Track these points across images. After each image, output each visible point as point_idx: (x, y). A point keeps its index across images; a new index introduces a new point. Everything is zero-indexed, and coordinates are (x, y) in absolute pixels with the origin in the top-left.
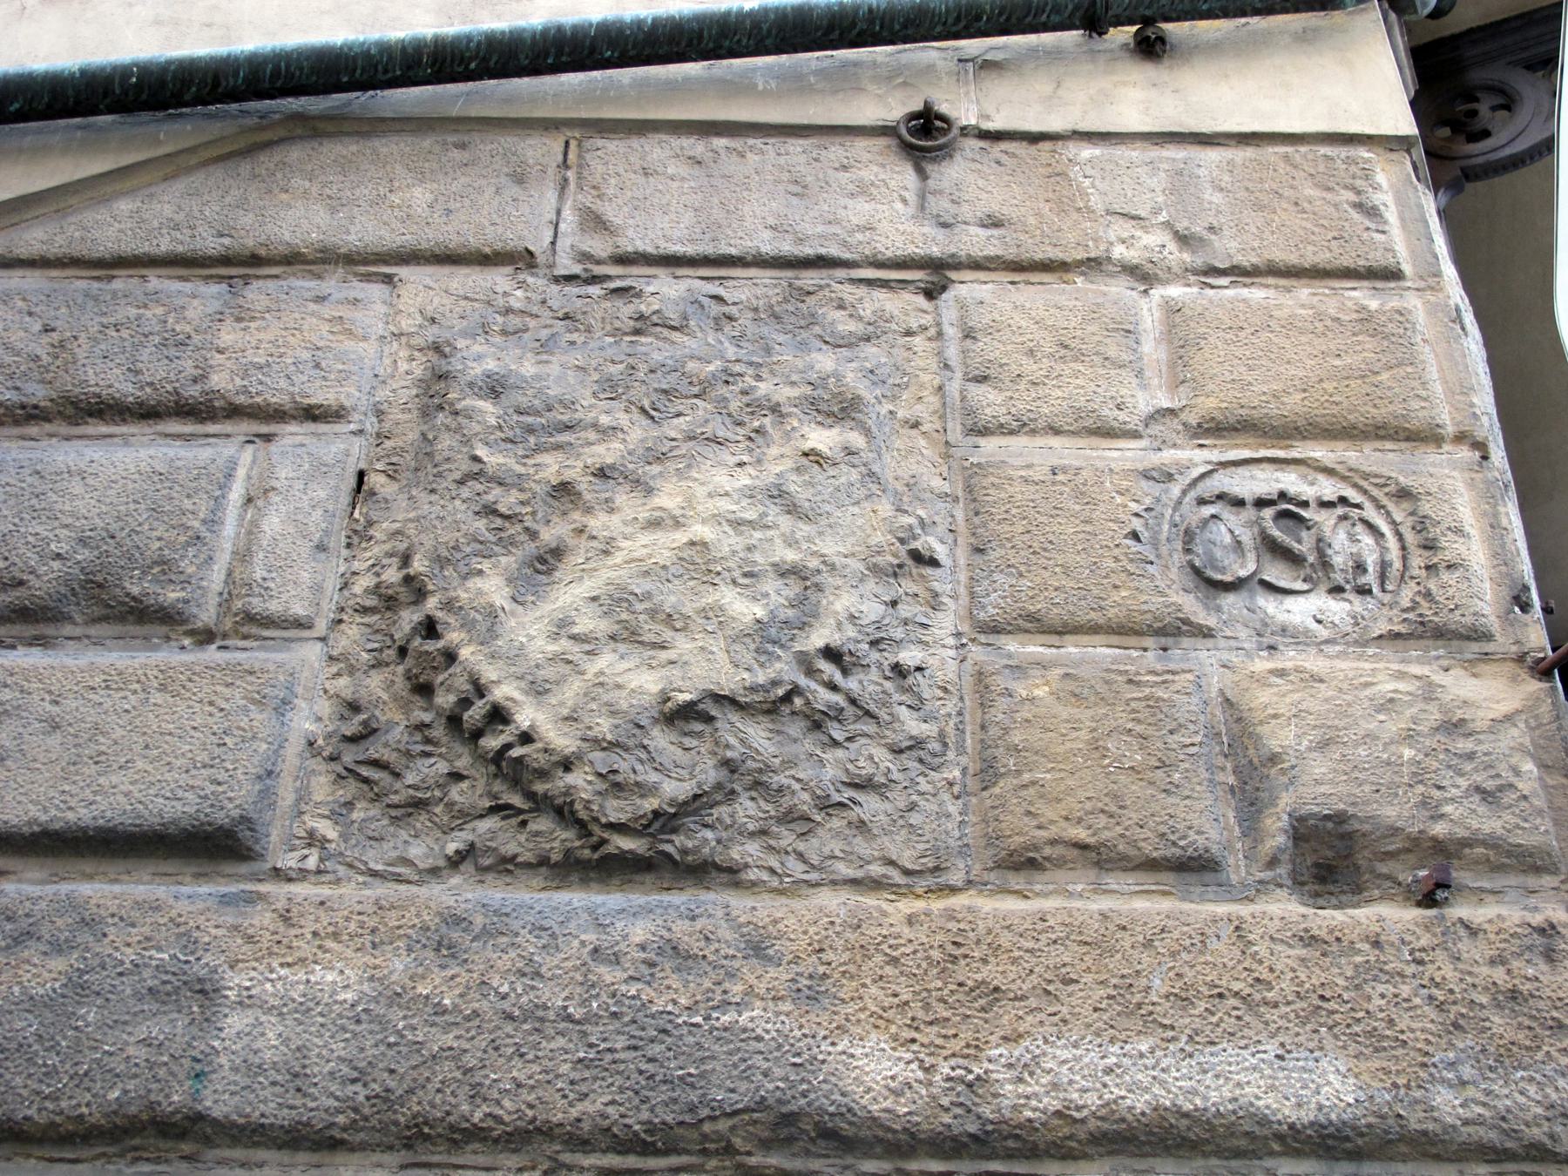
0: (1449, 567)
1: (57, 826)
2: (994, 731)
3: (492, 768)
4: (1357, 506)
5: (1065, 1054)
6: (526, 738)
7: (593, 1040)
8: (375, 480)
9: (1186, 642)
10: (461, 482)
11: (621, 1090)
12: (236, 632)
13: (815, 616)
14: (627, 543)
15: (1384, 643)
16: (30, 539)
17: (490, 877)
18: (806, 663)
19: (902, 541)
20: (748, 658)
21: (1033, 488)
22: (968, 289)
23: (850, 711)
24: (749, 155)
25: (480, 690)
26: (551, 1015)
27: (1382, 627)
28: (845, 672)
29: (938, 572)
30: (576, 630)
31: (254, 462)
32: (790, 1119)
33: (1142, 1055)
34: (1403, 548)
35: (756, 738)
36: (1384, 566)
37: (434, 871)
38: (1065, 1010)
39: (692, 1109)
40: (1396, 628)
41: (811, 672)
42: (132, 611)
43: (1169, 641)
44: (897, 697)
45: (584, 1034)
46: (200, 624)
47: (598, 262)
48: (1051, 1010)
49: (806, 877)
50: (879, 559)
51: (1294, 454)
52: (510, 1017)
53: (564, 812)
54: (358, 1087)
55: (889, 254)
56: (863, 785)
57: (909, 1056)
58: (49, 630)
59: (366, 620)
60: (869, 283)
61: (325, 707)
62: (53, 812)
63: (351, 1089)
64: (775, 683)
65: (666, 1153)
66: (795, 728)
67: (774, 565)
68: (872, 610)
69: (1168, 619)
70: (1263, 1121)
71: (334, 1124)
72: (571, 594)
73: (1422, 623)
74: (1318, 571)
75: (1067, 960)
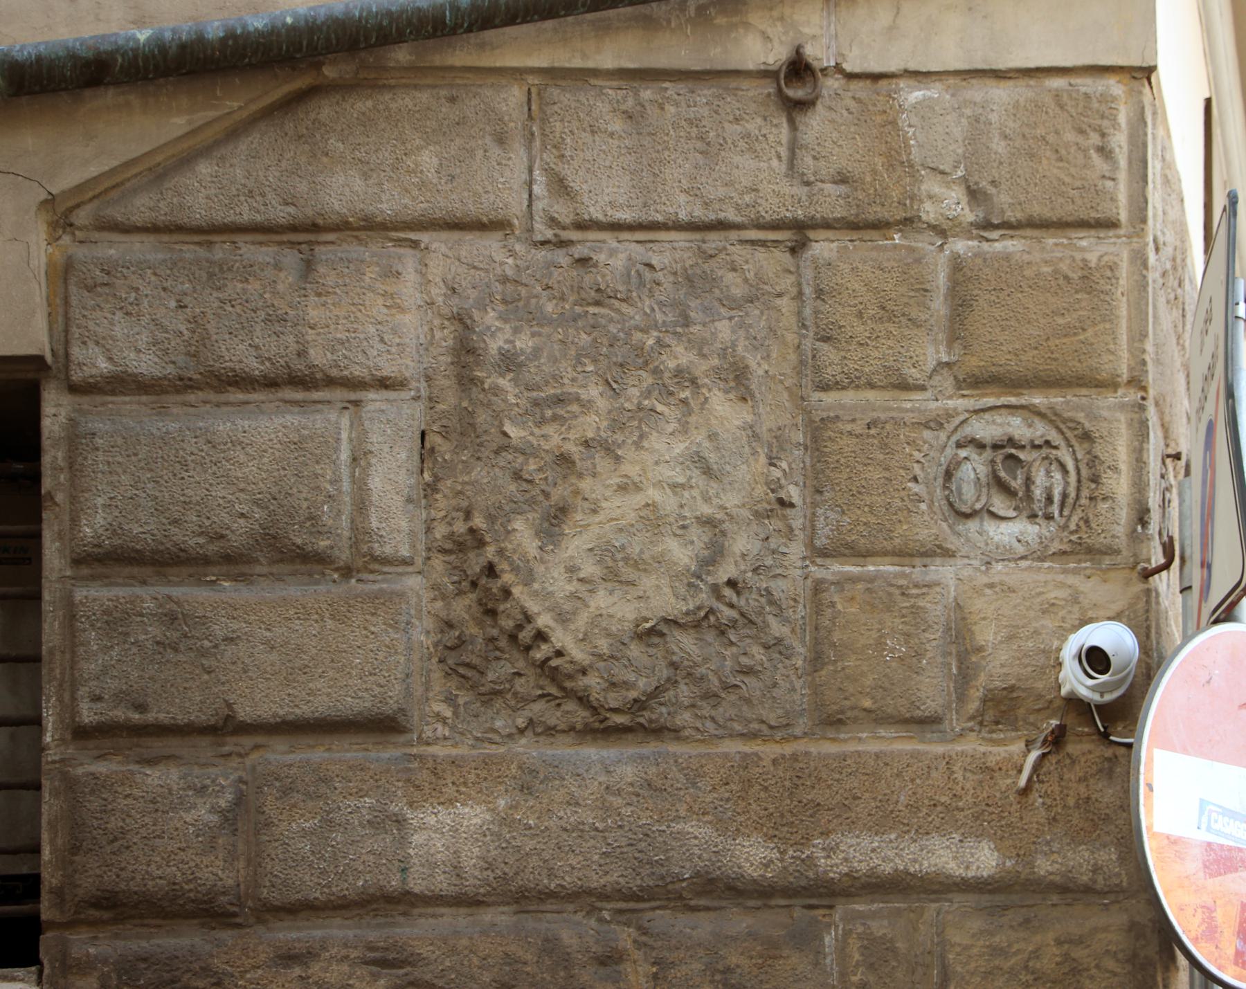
1: (291, 717)
2: (823, 633)
3: (539, 671)
4: (1056, 448)
5: (854, 841)
6: (559, 653)
7: (610, 841)
8: (433, 439)
9: (938, 560)
10: (497, 452)
11: (626, 869)
12: (366, 568)
13: (722, 555)
14: (608, 508)
16: (221, 501)
17: (541, 738)
18: (715, 590)
19: (773, 491)
20: (682, 591)
22: (823, 247)
23: (741, 621)
24: (667, 107)
25: (528, 618)
26: (587, 828)
27: (1055, 546)
28: (738, 593)
29: (794, 510)
30: (582, 575)
31: (352, 425)
32: (712, 881)
33: (891, 841)
34: (1079, 481)
35: (685, 644)
36: (1065, 496)
37: (510, 736)
38: (853, 815)
39: (663, 878)
41: (720, 597)
42: (298, 556)
43: (927, 560)
44: (768, 609)
45: (605, 838)
46: (342, 563)
47: (564, 228)
48: (846, 816)
49: (716, 732)
50: (759, 507)
51: (1023, 401)
52: (565, 830)
53: (582, 699)
54: (489, 872)
55: (768, 218)
56: (747, 671)
57: (772, 845)
58: (245, 569)
59: (447, 558)
60: (753, 242)
61: (429, 623)
62: (286, 709)
63: (485, 873)
64: (699, 608)
65: (649, 900)
66: (710, 636)
67: (697, 518)
68: (755, 547)
70: (949, 876)
71: (478, 894)
72: (576, 545)
74: (1025, 503)
75: (856, 785)
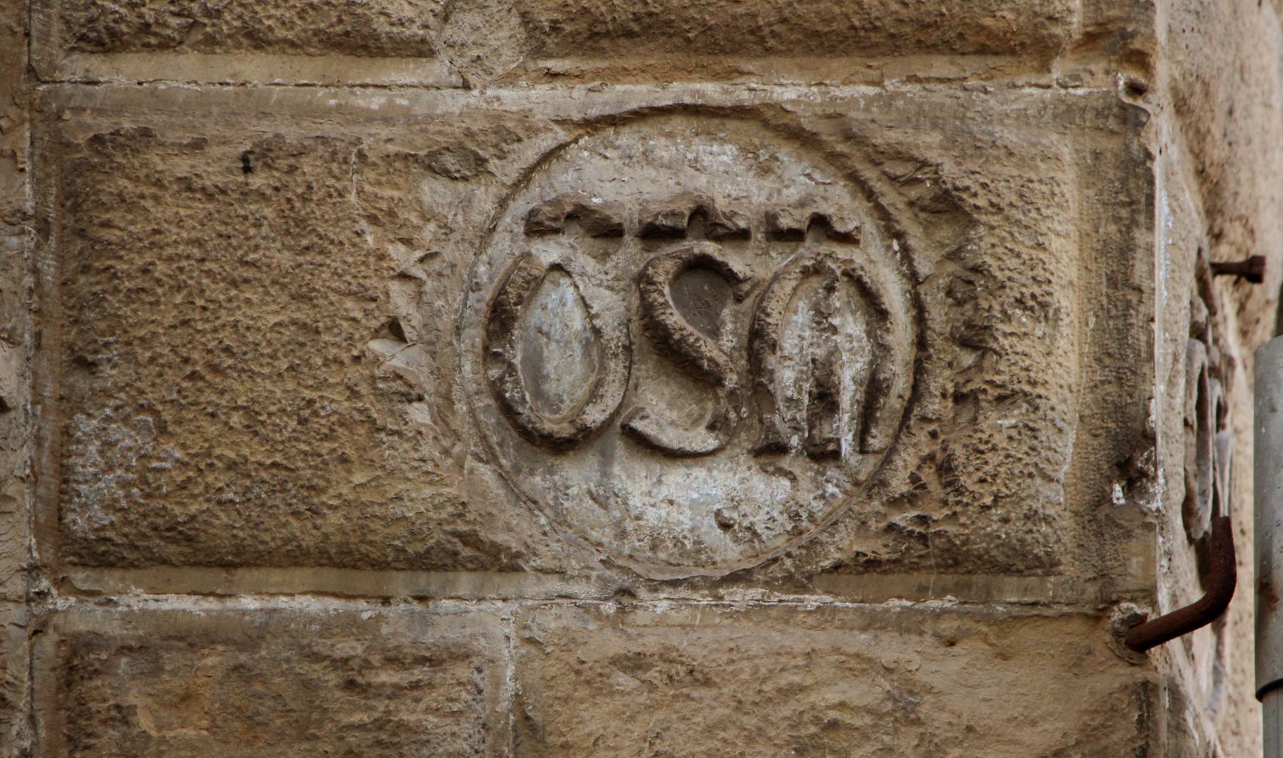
0: (1000, 399)
4: (847, 239)
9: (465, 582)
15: (842, 579)
21: (201, 207)
27: (844, 544)
34: (921, 343)
36: (874, 388)
40: (868, 547)
43: (432, 581)
69: (438, 536)
73: (923, 538)
74: (743, 407)
